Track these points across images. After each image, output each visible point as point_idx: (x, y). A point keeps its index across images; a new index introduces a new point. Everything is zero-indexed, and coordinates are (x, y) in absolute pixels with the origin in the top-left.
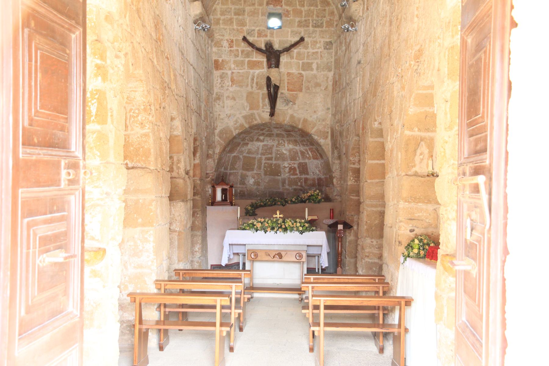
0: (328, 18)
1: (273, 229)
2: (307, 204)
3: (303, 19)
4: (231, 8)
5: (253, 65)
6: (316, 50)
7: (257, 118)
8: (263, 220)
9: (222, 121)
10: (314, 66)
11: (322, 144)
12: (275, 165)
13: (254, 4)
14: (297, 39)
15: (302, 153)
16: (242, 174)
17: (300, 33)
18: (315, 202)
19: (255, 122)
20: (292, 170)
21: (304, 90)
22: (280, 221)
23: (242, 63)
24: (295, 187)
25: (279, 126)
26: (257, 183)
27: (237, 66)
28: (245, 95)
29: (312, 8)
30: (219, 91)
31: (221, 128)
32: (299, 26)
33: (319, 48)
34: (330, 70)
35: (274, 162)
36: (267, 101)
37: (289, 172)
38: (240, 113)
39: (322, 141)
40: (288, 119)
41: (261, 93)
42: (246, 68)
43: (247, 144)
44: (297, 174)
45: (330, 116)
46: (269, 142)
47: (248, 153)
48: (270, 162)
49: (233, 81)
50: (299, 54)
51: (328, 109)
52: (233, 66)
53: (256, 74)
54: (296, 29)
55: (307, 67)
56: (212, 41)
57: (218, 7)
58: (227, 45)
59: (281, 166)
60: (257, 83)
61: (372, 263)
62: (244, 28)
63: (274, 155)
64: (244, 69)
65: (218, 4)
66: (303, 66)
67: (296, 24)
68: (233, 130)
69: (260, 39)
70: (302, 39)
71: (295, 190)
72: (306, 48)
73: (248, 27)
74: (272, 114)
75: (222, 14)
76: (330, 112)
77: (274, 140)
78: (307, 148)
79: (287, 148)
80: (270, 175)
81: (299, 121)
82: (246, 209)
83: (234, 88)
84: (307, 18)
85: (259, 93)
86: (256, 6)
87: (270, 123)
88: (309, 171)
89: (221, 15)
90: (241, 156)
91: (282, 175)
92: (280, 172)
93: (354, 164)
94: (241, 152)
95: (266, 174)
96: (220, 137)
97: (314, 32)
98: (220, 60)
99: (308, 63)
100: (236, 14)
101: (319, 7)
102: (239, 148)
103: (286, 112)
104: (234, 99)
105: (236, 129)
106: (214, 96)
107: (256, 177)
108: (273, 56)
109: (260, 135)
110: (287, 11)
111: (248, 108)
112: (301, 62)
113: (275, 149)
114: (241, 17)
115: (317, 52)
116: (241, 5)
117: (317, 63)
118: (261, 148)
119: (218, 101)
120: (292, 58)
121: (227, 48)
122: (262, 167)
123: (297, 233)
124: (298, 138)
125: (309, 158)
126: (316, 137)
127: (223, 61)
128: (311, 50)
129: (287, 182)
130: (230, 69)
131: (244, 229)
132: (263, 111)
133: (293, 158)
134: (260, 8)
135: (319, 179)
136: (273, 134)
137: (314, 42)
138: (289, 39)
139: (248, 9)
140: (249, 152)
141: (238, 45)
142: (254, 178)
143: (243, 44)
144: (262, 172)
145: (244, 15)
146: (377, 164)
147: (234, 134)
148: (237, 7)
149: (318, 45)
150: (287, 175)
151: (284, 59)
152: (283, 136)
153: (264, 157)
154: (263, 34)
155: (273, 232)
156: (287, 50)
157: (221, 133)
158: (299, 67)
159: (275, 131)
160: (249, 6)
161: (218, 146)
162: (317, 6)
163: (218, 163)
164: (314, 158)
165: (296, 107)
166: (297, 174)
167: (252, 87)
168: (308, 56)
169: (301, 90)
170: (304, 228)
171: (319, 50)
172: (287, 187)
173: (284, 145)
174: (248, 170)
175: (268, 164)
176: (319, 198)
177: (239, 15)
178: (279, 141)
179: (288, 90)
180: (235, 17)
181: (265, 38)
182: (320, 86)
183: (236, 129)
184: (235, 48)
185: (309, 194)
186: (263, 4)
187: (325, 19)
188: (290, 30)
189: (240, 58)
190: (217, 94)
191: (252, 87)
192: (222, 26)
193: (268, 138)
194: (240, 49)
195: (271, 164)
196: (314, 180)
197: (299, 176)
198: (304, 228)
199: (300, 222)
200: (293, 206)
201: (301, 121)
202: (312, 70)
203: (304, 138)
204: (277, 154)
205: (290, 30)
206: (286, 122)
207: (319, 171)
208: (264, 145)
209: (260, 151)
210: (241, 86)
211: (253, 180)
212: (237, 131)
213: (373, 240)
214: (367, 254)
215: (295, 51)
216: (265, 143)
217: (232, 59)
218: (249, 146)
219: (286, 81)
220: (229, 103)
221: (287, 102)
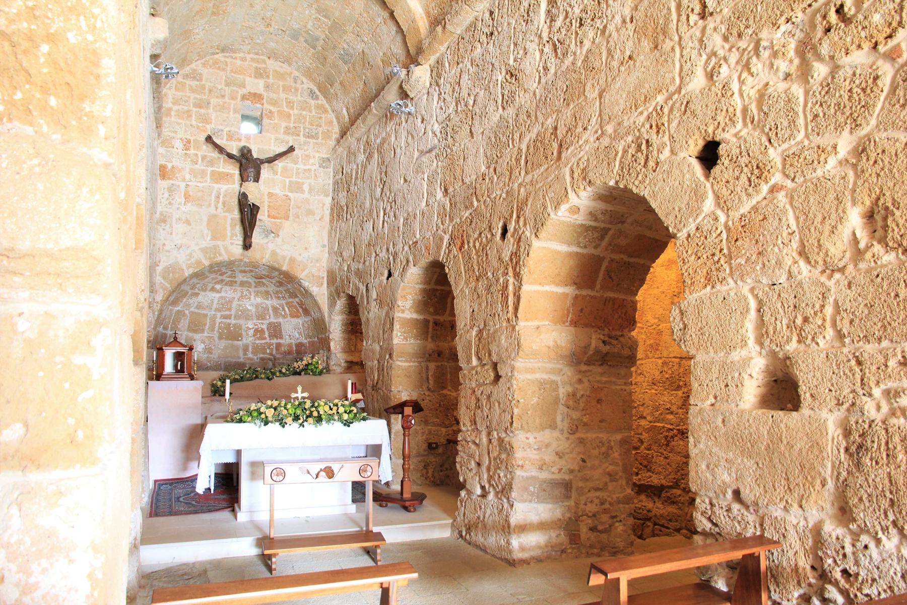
0: (325, 128)
1: (296, 418)
2: (303, 378)
3: (292, 125)
4: (189, 97)
5: (219, 177)
6: (309, 167)
7: (223, 252)
8: (276, 403)
9: (168, 254)
10: (306, 187)
11: (314, 294)
12: (235, 325)
13: (223, 96)
14: (283, 149)
15: (275, 309)
16: (187, 336)
17: (287, 142)
18: (314, 374)
19: (220, 259)
20: (259, 332)
21: (291, 218)
22: (308, 404)
23: (203, 172)
24: (262, 356)
25: (254, 265)
26: (209, 351)
27: (195, 177)
28: (205, 219)
29: (304, 113)
30: (165, 209)
31: (166, 264)
32: (286, 133)
33: (313, 164)
34: (328, 195)
35: (233, 321)
36: (238, 229)
37: (254, 335)
38: (197, 244)
39: (314, 290)
40: (267, 256)
41: (229, 218)
42: (209, 180)
43: (197, 295)
44: (265, 339)
45: (327, 255)
46: (228, 293)
47: (197, 308)
48: (228, 321)
49: (187, 197)
50: (285, 169)
51: (324, 246)
52: (188, 177)
53: (223, 191)
54: (282, 136)
55: (296, 187)
56: (159, 135)
57: (169, 92)
58: (182, 146)
59: (243, 327)
60: (224, 203)
61: (527, 478)
62: (208, 126)
63: (233, 312)
64: (206, 181)
65: (170, 89)
66: (290, 186)
67: (282, 131)
68: (185, 268)
69: (229, 143)
70: (291, 149)
71: (262, 359)
72: (296, 163)
73: (213, 126)
74: (247, 246)
75: (176, 102)
76: (327, 249)
77: (235, 291)
78: (284, 302)
79: (253, 302)
80: (227, 338)
81: (284, 260)
82: (213, 385)
83: (190, 207)
84: (296, 125)
85: (226, 217)
86: (227, 99)
87: (241, 260)
88: (283, 333)
89: (174, 104)
90: (187, 312)
91: (244, 339)
92: (241, 335)
93: (403, 312)
94: (189, 305)
95: (220, 338)
96: (164, 278)
97: (305, 143)
98: (169, 166)
99: (297, 183)
100: (196, 106)
101: (314, 113)
102: (185, 300)
103: (267, 247)
104: (188, 222)
105: (189, 267)
106: (158, 215)
107: (207, 342)
108: (248, 165)
109: (216, 283)
110: (270, 112)
111: (209, 238)
112: (287, 180)
113: (235, 303)
114: (203, 111)
115: (310, 170)
116: (205, 94)
117: (310, 185)
118: (216, 302)
119: (163, 225)
120: (276, 173)
121: (180, 151)
122: (216, 329)
123: (338, 425)
124: (272, 288)
125: (284, 317)
126: (306, 284)
127: (173, 167)
128: (301, 166)
129: (250, 349)
130: (184, 180)
131: (240, 421)
132: (232, 244)
133: (261, 317)
134: (233, 102)
135: (299, 345)
136: (236, 282)
137: (306, 156)
138: (272, 148)
139: (214, 101)
140: (199, 307)
141: (198, 148)
142: (204, 343)
143: (204, 147)
144: (216, 335)
145: (208, 108)
146: (538, 292)
147: (187, 275)
148: (198, 96)
149: (312, 161)
150: (251, 339)
151: (265, 172)
152: (249, 284)
153: (219, 314)
154: (236, 137)
155: (296, 425)
156: (270, 160)
157: (166, 271)
158: (285, 186)
159: (240, 277)
160: (217, 97)
161: (161, 290)
162: (310, 111)
163: (159, 317)
164: (292, 316)
165: (279, 240)
166: (265, 339)
167: (217, 208)
168: (298, 173)
169: (287, 218)
170: (352, 415)
171: (313, 168)
172: (250, 355)
173: (250, 298)
174: (195, 331)
175: (225, 324)
176: (321, 367)
177: (200, 107)
178: (242, 293)
179: (269, 216)
180: (195, 109)
181: (237, 143)
182: (314, 214)
183: (189, 267)
184: (192, 151)
185: (305, 362)
186: (237, 98)
187: (321, 129)
188: (273, 137)
189: (200, 166)
190: (161, 214)
191: (217, 208)
192: (173, 119)
193: (228, 288)
194: (200, 154)
195: (229, 324)
196: (290, 345)
197: (268, 340)
198: (352, 415)
199: (343, 406)
200: (284, 379)
201: (287, 260)
202: (303, 192)
203: (281, 289)
204: (238, 310)
205: (273, 137)
206: (264, 261)
207: (300, 334)
208: (221, 297)
209: (215, 306)
210: (200, 206)
211: (203, 346)
212: (191, 271)
213: (529, 435)
214: (520, 463)
215: (279, 164)
216: (223, 294)
217: (188, 166)
218: (200, 298)
219: (266, 204)
220: (179, 228)
221: (268, 232)
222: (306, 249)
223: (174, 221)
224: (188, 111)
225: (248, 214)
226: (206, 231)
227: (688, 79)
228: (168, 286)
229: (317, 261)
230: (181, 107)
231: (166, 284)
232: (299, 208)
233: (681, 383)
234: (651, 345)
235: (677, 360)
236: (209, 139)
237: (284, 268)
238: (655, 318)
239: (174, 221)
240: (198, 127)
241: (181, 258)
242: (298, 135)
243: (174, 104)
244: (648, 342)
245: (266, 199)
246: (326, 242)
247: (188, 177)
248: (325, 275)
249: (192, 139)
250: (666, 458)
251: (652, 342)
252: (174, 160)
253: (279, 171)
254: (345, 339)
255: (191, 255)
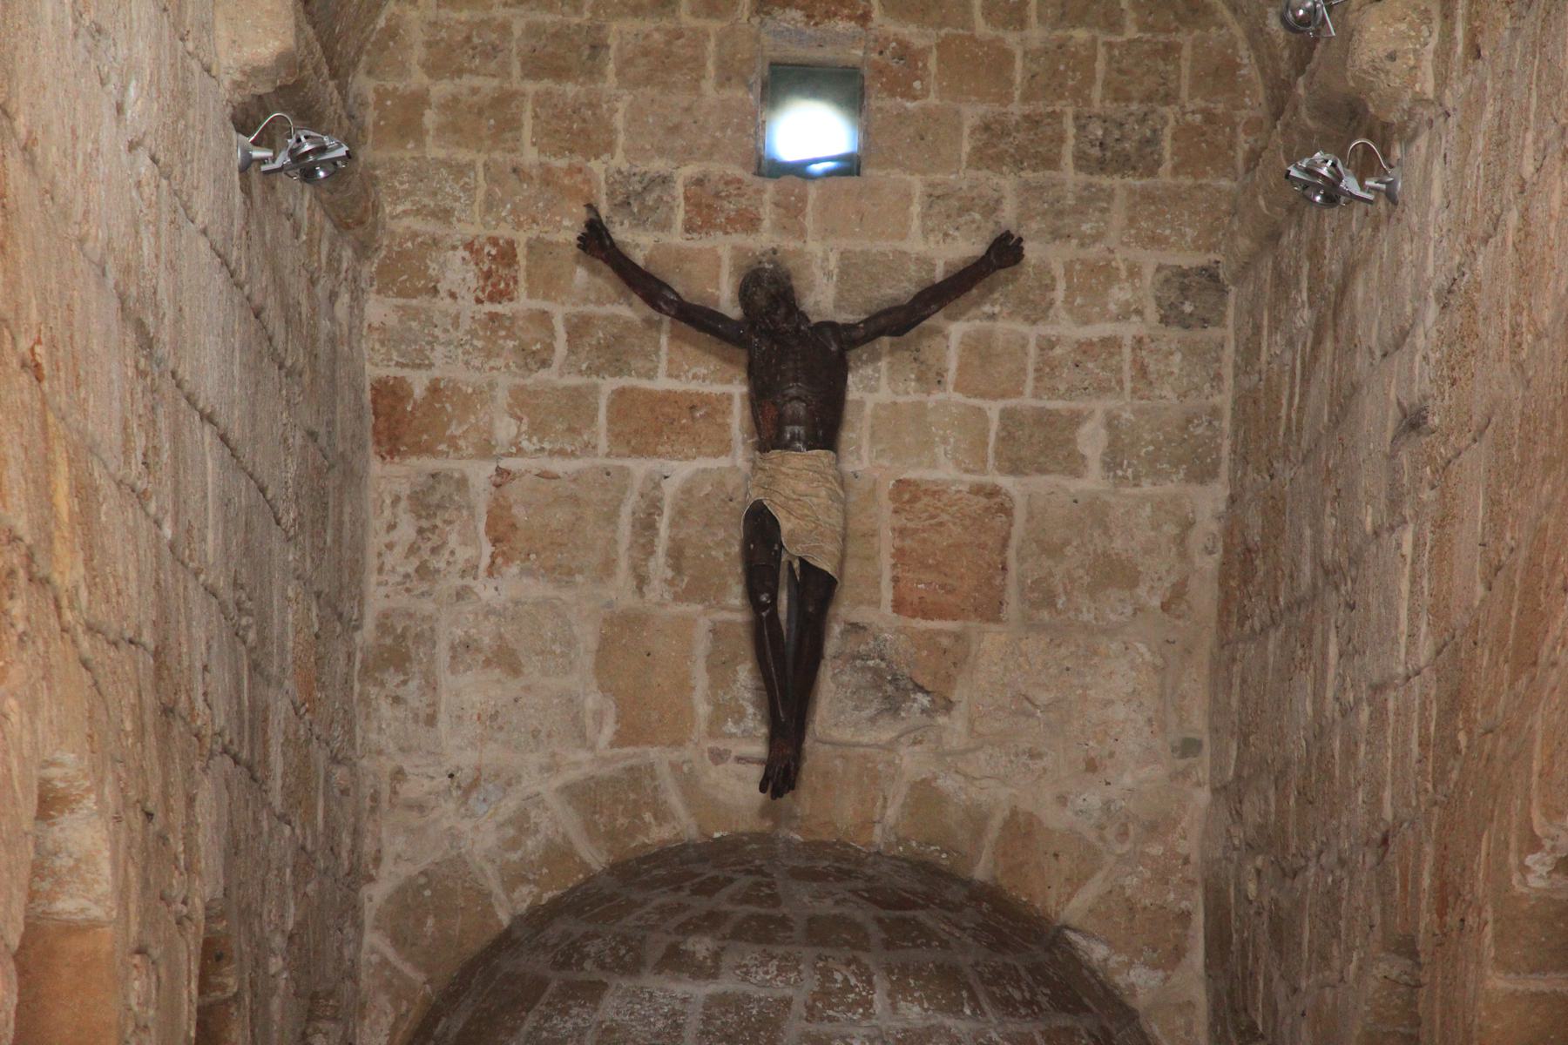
0: (1192, 105)
3: (1017, 109)
4: (505, 28)
5: (651, 423)
9: (414, 819)
10: (1091, 440)
14: (967, 246)
19: (659, 834)
21: (1013, 606)
23: (577, 404)
27: (538, 429)
28: (587, 637)
29: (1081, 34)
30: (402, 601)
31: (407, 870)
32: (985, 157)
33: (1128, 312)
38: (551, 768)
40: (892, 813)
41: (704, 624)
42: (603, 443)
43: (594, 991)
45: (1203, 796)
49: (501, 531)
50: (980, 350)
51: (1189, 747)
52: (505, 429)
53: (670, 490)
54: (961, 178)
55: (1040, 442)
60: (676, 555)
62: (597, 166)
64: (589, 448)
68: (494, 885)
69: (700, 243)
70: (1005, 252)
72: (1036, 310)
73: (619, 160)
74: (781, 776)
76: (1202, 768)
81: (978, 832)
83: (511, 586)
84: (1042, 107)
89: (434, 69)
96: (398, 940)
98: (419, 382)
99: (1044, 419)
100: (536, 67)
101: (1131, 32)
104: (506, 659)
105: (513, 879)
108: (793, 362)
109: (685, 929)
110: (905, 52)
111: (608, 731)
112: (993, 409)
114: (571, 89)
115: (1111, 344)
117: (1111, 423)
119: (392, 679)
120: (931, 378)
121: (467, 305)
127: (434, 389)
128: (1065, 328)
130: (486, 450)
132: (718, 757)
136: (783, 923)
137: (1093, 269)
138: (916, 245)
141: (547, 284)
143: (581, 274)
145: (593, 72)
147: (505, 918)
149: (1120, 294)
151: (873, 387)
154: (730, 207)
156: (902, 321)
157: (408, 902)
159: (803, 901)
161: (383, 1000)
167: (641, 581)
168: (1047, 369)
169: (992, 610)
171: (1128, 331)
173: (867, 1004)
177: (560, 73)
178: (827, 974)
179: (898, 606)
180: (530, 87)
181: (739, 239)
182: (1133, 581)
183: (513, 879)
184: (523, 302)
187: (1170, 112)
188: (917, 184)
190: (383, 627)
191: (641, 581)
193: (751, 954)
194: (560, 313)
202: (1074, 465)
205: (917, 184)
208: (721, 1000)
210: (562, 574)
212: (526, 897)
216: (728, 984)
217: (505, 380)
218: (610, 1008)
219: (886, 545)
220: (470, 690)
222: (1092, 766)
223: (443, 653)
224: (504, 99)
225: (789, 622)
226: (592, 701)
228: (419, 977)
230: (467, 81)
231: (407, 969)
232: (1053, 550)
236: (595, 240)
237: (981, 872)
239: (443, 653)
240: (548, 177)
241: (479, 835)
242: (1052, 162)
243: (434, 69)
245: (884, 518)
247: (505, 429)
249: (522, 238)
252: (438, 354)
253: (952, 365)
255: (521, 823)
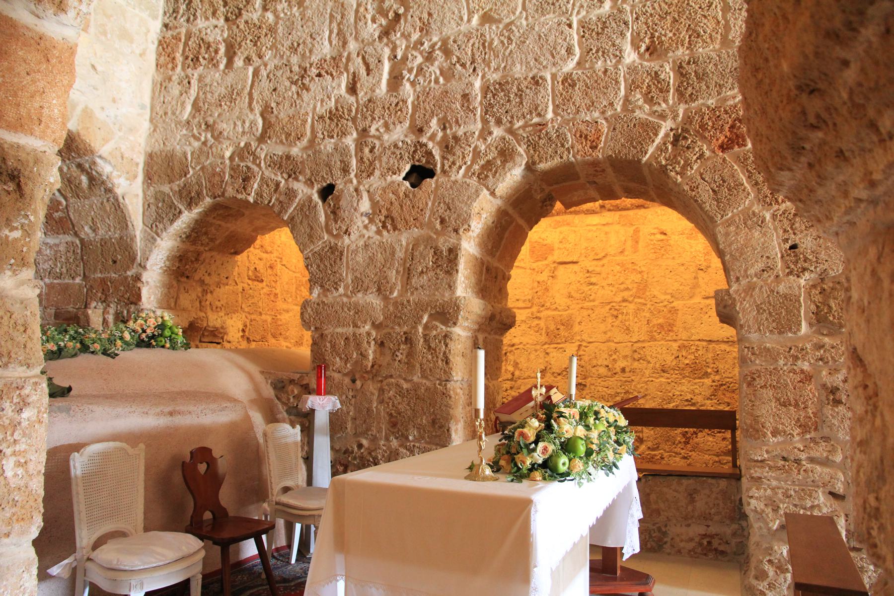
222: (114, 101)
227: (687, 232)
229: (131, 130)
233: (709, 370)
234: (661, 326)
235: (704, 344)
238: (666, 293)
244: (655, 321)
246: (147, 100)
248: (141, 160)
250: (685, 458)
251: (661, 321)
254: (164, 285)
